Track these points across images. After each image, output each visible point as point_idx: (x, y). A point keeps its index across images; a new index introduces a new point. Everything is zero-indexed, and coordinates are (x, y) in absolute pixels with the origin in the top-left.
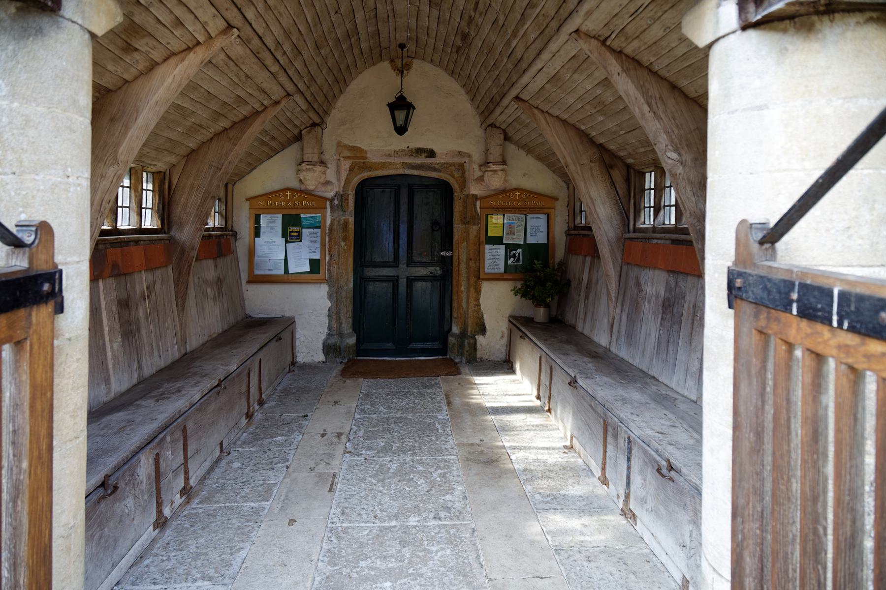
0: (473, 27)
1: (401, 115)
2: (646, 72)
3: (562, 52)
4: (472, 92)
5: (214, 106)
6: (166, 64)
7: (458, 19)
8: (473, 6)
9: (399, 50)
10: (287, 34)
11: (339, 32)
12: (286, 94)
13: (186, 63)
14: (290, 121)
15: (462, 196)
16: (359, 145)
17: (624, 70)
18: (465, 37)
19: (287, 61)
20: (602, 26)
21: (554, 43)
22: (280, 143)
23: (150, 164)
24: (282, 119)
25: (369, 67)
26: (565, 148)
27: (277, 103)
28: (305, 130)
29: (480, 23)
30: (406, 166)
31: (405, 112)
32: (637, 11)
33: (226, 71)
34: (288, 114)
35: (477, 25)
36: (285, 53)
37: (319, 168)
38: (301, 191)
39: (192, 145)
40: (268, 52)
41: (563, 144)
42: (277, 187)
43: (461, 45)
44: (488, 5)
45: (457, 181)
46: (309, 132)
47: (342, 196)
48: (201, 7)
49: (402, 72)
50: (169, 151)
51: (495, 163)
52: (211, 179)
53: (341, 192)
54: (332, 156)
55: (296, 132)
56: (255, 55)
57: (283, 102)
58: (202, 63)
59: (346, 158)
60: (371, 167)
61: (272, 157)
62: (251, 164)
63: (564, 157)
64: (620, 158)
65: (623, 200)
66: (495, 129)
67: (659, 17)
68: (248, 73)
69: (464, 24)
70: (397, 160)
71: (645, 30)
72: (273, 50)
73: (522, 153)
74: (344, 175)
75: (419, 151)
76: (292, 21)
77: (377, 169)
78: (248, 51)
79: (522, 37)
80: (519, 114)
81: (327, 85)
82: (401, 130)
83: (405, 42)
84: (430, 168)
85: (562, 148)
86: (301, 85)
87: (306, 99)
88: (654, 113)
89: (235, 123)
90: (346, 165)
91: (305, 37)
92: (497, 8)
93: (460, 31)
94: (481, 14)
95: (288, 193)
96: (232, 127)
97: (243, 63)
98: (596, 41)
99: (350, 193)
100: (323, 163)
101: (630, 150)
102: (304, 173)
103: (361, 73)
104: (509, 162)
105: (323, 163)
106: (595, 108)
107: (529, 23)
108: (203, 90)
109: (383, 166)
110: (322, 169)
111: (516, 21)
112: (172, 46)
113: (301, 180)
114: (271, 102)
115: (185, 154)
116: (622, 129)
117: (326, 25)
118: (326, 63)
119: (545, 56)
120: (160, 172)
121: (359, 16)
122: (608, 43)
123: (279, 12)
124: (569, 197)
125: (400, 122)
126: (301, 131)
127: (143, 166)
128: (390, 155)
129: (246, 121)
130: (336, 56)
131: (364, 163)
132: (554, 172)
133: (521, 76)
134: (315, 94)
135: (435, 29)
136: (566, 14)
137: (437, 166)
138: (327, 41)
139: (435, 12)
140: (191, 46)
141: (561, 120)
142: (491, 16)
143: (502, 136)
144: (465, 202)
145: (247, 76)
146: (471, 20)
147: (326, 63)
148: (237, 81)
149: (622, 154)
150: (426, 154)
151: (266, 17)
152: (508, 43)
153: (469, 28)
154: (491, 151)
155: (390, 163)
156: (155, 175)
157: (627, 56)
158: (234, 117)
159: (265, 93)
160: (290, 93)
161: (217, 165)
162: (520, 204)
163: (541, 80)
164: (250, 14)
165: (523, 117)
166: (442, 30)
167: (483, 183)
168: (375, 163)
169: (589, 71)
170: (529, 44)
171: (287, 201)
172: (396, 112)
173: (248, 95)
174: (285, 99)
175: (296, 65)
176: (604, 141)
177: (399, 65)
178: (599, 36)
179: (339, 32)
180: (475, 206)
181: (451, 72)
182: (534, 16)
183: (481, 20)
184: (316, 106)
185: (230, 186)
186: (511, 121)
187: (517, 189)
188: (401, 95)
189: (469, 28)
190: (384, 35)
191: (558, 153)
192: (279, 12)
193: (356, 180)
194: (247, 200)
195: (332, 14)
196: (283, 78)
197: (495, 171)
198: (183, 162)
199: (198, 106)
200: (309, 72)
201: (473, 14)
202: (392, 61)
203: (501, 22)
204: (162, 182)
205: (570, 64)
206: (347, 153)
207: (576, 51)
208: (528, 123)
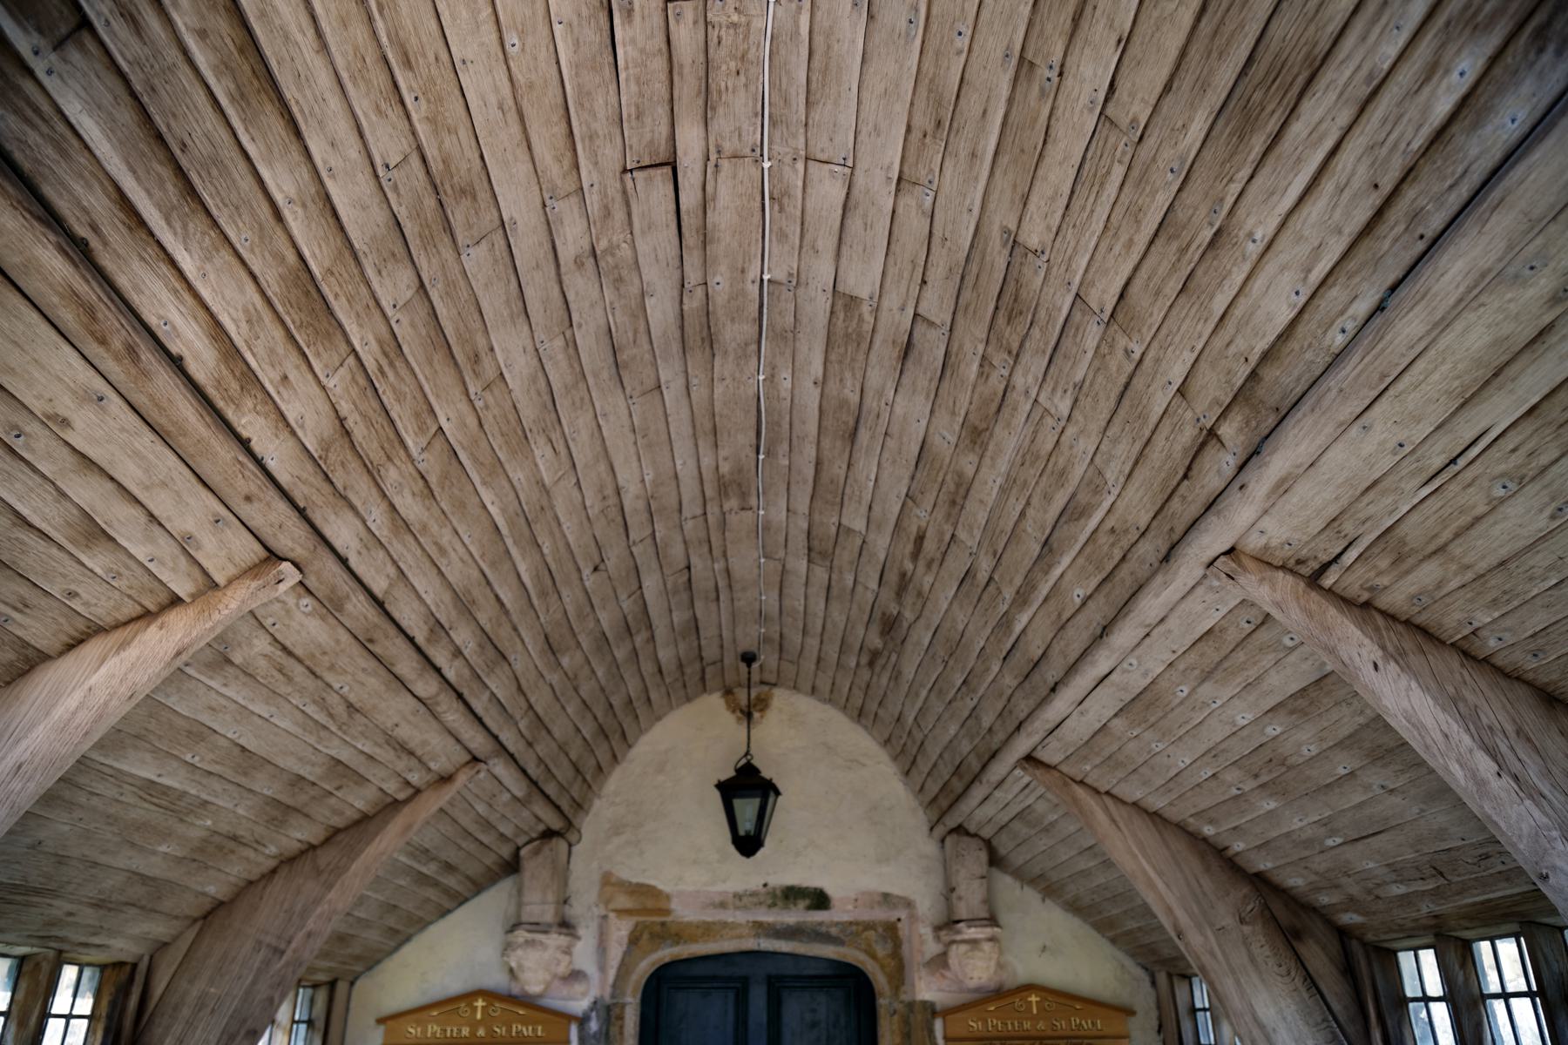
0: (909, 599)
1: (747, 809)
2: (1455, 661)
3: (1172, 623)
4: (907, 757)
5: (265, 786)
6: (70, 659)
7: (874, 585)
8: (910, 547)
9: (743, 667)
10: (464, 605)
11: (604, 617)
12: (468, 757)
13: (131, 653)
14: (487, 825)
15: (897, 1006)
16: (652, 882)
17: (1388, 656)
18: (889, 625)
19: (466, 672)
20: (1318, 524)
21: (1157, 596)
22: (468, 877)
23: (86, 945)
24: (466, 821)
25: (678, 706)
26: (1167, 885)
27: (445, 779)
28: (529, 847)
29: (926, 588)
30: (761, 929)
31: (756, 802)
32: (1453, 461)
33: (284, 689)
34: (481, 808)
35: (920, 594)
36: (458, 653)
37: (556, 940)
38: (511, 999)
39: (215, 888)
40: (400, 642)
41: (1160, 874)
42: (455, 986)
43: (880, 646)
44: (947, 537)
45: (882, 967)
46: (537, 852)
47: (608, 1009)
48: (164, 484)
49: (749, 716)
50: (142, 908)
51: (972, 922)
52: (254, 983)
53: (608, 1000)
54: (589, 908)
55: (506, 851)
56: (365, 644)
57: (462, 778)
58: (178, 654)
59: (621, 912)
60: (675, 934)
61: (449, 911)
62: (397, 932)
63: (1169, 910)
64: (1315, 910)
65: (1350, 1029)
66: (966, 839)
67: (1544, 470)
68: (352, 698)
69: (887, 594)
70: (741, 917)
71: (1478, 519)
72: (420, 639)
73: (1031, 896)
74: (616, 953)
75: (791, 894)
76: (476, 574)
77: (693, 939)
78: (345, 637)
79: (1046, 600)
80: (1030, 801)
81: (579, 741)
82: (748, 844)
83: (754, 649)
84: (818, 934)
85: (1160, 885)
86: (508, 737)
87: (524, 772)
88: (1516, 778)
89: (337, 831)
90: (621, 930)
91: (515, 617)
92: (972, 543)
93: (877, 615)
94: (929, 565)
95: (480, 1003)
96: (327, 841)
97: (332, 668)
98: (1290, 578)
99: (629, 999)
100: (566, 925)
101: (1355, 890)
102: (519, 952)
103: (659, 719)
104: (1003, 918)
105: (566, 925)
106: (1256, 776)
107: (1066, 561)
108: (222, 742)
109: (708, 930)
110: (563, 940)
111: (1028, 563)
112: (86, 604)
113: (511, 970)
114: (429, 777)
115: (196, 914)
116: (1333, 833)
117: (570, 596)
118: (576, 689)
119: (1124, 636)
120: (119, 965)
121: (651, 584)
122: (1328, 581)
123: (436, 544)
124: (1159, 1007)
125: (746, 825)
126: (518, 849)
127: (60, 952)
128: (722, 905)
129: (364, 824)
130: (600, 674)
131: (663, 924)
132: (1113, 941)
133: (1044, 702)
134: (548, 761)
135: (821, 614)
136: (1195, 509)
137: (834, 931)
138: (574, 635)
139: (820, 574)
140: (152, 607)
141: (1146, 811)
142: (956, 565)
143: (983, 856)
144: (906, 1021)
145: (350, 706)
146: (904, 582)
147: (576, 689)
148: (321, 718)
149: (1324, 899)
150: (807, 902)
151: (396, 548)
152: (1005, 622)
153: (900, 604)
154: (962, 890)
155: (725, 924)
156: (108, 971)
157: (1390, 617)
158: (327, 815)
159: (411, 753)
160: (480, 755)
161: (274, 942)
162: (1041, 1025)
163: (1102, 707)
164: (343, 533)
165: (1041, 807)
166: (838, 616)
167: (948, 974)
168: (689, 924)
169: (1253, 673)
170: (1065, 616)
171: (474, 1025)
172: (738, 803)
173: (362, 758)
174: (466, 770)
175: (493, 687)
176: (1269, 865)
177: (744, 702)
178: (1299, 562)
179: (606, 618)
180: (931, 1031)
181: (856, 713)
182: (1083, 539)
183: (929, 579)
184: (551, 789)
185: (342, 987)
186: (1006, 819)
187: (1029, 988)
188: (749, 762)
189: (900, 604)
190: (708, 632)
191: (1151, 899)
192: (436, 544)
193: (645, 967)
194: (381, 1021)
195: (586, 572)
196: (453, 715)
197: (974, 943)
198: (190, 935)
199: (217, 785)
200: (531, 707)
201: (909, 566)
202: (728, 692)
203: (982, 576)
204: (124, 990)
205: (1192, 657)
206: (623, 901)
207: (1219, 615)
208: (1052, 824)
